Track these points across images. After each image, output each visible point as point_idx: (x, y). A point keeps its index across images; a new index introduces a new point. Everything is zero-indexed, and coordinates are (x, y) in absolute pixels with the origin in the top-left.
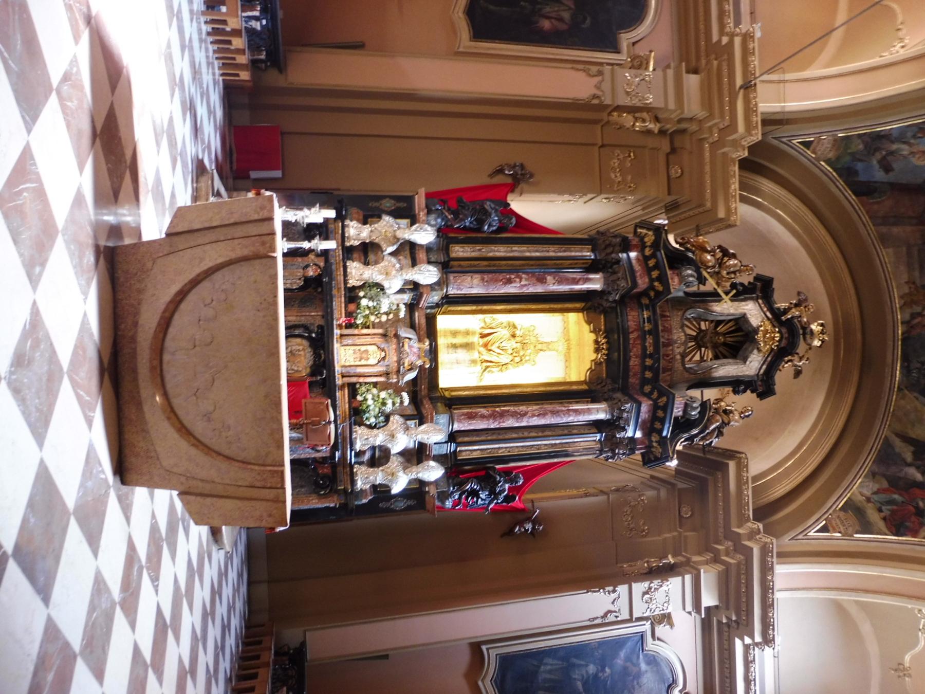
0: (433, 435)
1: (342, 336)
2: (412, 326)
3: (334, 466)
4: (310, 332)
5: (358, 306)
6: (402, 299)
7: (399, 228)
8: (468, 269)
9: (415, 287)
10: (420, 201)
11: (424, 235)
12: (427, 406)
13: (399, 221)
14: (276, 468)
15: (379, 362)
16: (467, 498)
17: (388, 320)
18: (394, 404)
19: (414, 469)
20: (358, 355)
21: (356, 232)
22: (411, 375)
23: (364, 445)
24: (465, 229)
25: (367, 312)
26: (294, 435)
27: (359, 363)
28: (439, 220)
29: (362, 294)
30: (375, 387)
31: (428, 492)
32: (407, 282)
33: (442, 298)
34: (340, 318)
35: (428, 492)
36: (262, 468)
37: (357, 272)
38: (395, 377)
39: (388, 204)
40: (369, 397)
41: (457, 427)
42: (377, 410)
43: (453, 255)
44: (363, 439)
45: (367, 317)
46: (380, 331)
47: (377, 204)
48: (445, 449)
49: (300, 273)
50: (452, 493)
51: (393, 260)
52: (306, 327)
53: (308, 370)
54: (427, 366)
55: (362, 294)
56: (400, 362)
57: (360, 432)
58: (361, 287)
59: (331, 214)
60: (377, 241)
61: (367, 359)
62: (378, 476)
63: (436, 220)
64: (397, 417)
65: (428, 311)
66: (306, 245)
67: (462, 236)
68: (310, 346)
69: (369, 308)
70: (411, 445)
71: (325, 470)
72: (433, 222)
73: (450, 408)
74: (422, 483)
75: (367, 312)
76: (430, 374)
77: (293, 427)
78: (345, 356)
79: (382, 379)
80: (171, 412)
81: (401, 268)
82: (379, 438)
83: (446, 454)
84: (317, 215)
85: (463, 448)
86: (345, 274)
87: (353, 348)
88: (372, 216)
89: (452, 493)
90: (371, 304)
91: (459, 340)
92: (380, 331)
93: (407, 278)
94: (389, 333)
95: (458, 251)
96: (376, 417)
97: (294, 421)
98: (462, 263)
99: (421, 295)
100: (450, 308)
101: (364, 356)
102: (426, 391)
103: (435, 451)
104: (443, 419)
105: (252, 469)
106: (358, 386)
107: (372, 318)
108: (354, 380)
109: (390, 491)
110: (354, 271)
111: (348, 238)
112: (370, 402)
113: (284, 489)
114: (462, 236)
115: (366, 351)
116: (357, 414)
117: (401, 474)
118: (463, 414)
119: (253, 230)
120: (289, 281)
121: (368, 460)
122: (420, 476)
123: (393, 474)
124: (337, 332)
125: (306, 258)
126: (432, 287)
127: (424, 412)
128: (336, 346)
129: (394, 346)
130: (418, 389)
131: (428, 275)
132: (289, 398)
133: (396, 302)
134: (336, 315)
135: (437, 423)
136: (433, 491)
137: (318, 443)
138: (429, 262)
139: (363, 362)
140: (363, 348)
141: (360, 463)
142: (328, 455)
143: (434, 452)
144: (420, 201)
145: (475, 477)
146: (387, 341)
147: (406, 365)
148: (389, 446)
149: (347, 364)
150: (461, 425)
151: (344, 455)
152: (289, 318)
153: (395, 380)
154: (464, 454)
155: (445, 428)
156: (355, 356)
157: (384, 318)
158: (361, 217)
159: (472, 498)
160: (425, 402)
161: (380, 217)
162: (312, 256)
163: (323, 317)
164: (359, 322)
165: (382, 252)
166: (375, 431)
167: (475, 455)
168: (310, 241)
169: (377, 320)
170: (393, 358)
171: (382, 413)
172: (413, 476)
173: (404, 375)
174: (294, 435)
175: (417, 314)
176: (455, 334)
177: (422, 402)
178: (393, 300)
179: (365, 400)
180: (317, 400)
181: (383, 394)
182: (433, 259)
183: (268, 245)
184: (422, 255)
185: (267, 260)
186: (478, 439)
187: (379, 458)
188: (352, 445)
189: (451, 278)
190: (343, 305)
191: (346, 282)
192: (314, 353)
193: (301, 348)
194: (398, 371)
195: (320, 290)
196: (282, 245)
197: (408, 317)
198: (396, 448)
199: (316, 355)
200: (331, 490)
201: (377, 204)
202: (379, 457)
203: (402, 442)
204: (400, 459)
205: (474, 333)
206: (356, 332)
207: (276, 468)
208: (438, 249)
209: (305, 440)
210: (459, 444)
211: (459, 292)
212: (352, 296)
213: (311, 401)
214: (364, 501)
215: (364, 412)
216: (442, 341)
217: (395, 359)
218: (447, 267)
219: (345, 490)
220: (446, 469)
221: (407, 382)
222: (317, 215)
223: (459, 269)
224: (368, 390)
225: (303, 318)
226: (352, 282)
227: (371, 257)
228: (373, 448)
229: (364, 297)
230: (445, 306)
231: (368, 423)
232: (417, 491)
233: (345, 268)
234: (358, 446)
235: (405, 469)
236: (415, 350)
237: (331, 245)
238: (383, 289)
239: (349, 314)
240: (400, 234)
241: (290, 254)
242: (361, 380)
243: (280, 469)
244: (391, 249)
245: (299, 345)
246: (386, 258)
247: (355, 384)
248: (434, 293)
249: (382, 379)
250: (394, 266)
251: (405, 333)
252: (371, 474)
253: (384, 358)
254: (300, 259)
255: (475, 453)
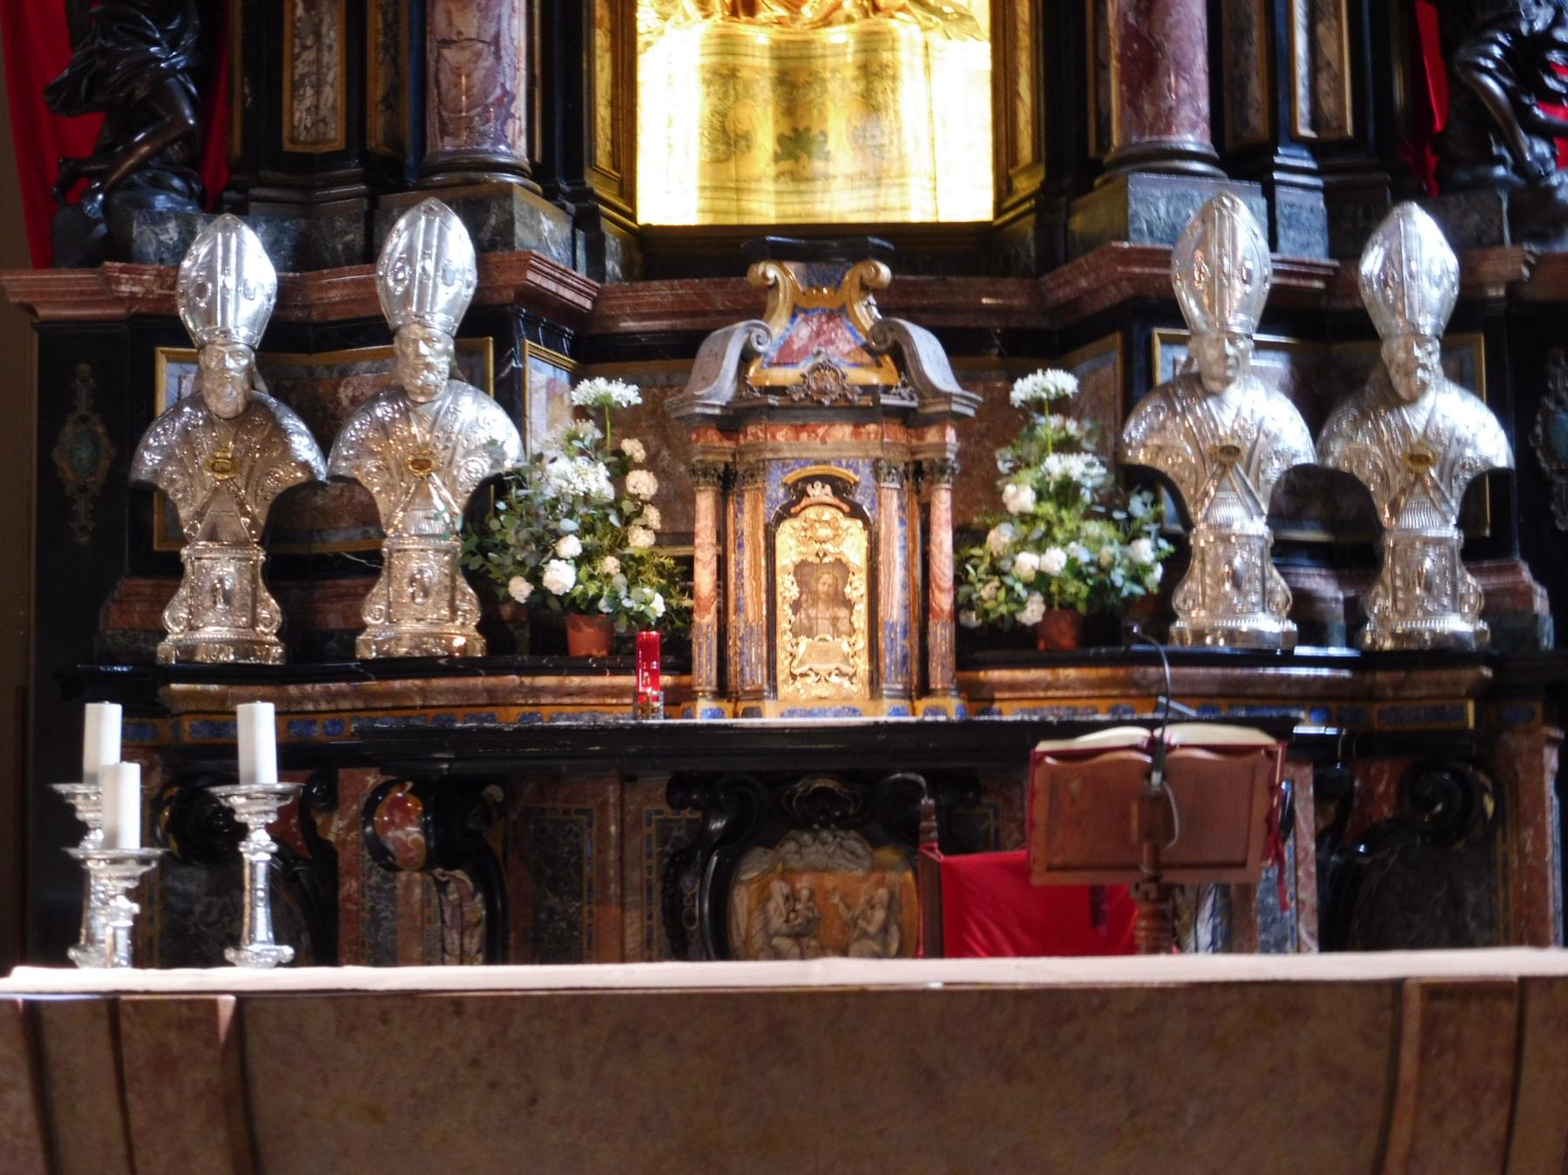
0: (1237, 250)
1: (723, 691)
2: (682, 347)
3: (1362, 744)
4: (703, 841)
5: (578, 607)
6: (552, 393)
7: (197, 401)
8: (408, 68)
9: (493, 335)
10: (63, 294)
11: (240, 276)
12: (1077, 281)
13: (163, 403)
14: (1412, 1027)
15: (855, 512)
16: (1549, 99)
17: (650, 464)
18: (1066, 446)
19: (1393, 351)
20: (822, 613)
21: (216, 608)
22: (929, 352)
23: (1266, 596)
24: (206, 70)
25: (610, 564)
26: (1204, 932)
27: (861, 608)
28: (161, 202)
29: (520, 589)
30: (979, 537)
31: (1513, 286)
32: (467, 368)
33: (550, 195)
34: (630, 698)
35: (1513, 286)
36: (1406, 1099)
37: (417, 607)
38: (932, 436)
39: (80, 455)
40: (1028, 562)
41: (1193, 138)
42: (1093, 528)
43: (335, 134)
44: (1241, 598)
45: (633, 568)
46: (705, 503)
47: (82, 507)
48: (1304, 200)
49: (412, 885)
50: (1520, 166)
51: (356, 429)
52: (679, 861)
53: (887, 855)
54: (885, 272)
55: (520, 589)
56: (861, 410)
57: (1199, 616)
58: (488, 589)
59: (105, 724)
60: (259, 511)
61: (841, 565)
62: (1430, 525)
63: (162, 218)
64: (1135, 430)
65: (612, 266)
66: (258, 849)
67: (242, 90)
68: (771, 843)
69: (586, 558)
70: (1276, 364)
71: (1381, 785)
72: (171, 233)
73: (1096, 168)
74: (1466, 317)
75: (610, 564)
76: (924, 264)
77: (1169, 939)
78: (822, 680)
79: (943, 502)
80: (838, 508)
81: (398, 393)
82: (1239, 519)
83: (1329, 193)
84: (113, 797)
85: (1302, 106)
86: (422, 666)
87: (784, 640)
88: (142, 531)
89: (1520, 166)
90: (571, 546)
91: (762, 123)
92: (705, 503)
93: (443, 364)
94: (715, 458)
95: (315, 107)
96: (1130, 535)
97: (1141, 927)
98: (377, 90)
99: (538, 300)
100: (603, 159)
101: (824, 583)
102: (1010, 284)
103: (1310, 245)
104: (1153, 203)
105: (1411, 1156)
106: (972, 620)
107: (640, 540)
108: (941, 637)
109: (1496, 475)
110: (408, 626)
111: (244, 646)
112: (1055, 559)
113: (1525, 982)
114: (242, 90)
115: (802, 570)
116: (1112, 629)
117: (1416, 419)
118: (1132, 101)
119: (90, 1115)
120: (453, 938)
121: (1342, 583)
122: (1428, 324)
123: (1419, 459)
124: (704, 712)
125: (344, 857)
126: (491, 245)
127: (1112, 296)
128: (771, 716)
129: (782, 435)
130: (997, 326)
131: (434, 263)
132: (1021, 951)
133: (567, 424)
134: (621, 715)
135: (1174, 233)
136: (1512, 261)
137: (1260, 812)
138: (370, 253)
139: (857, 588)
140: (788, 588)
141: (1356, 616)
142: (1307, 772)
143: (1317, 253)
144: (63, 294)
145: (1448, 50)
146: (757, 471)
147: (874, 378)
148: (1274, 471)
149: (862, 665)
150: (1186, 113)
151: (1316, 697)
152: (632, 943)
153: (951, 435)
154: (1328, 105)
155: (1199, 194)
156: (824, 625)
157: (642, 483)
158: (145, 584)
159: (1551, 70)
160: (1064, 293)
161: (148, 494)
162: (336, 828)
163: (628, 779)
164: (658, 606)
165: (312, 484)
166: (1201, 539)
167: (1339, 49)
168: (242, 831)
169: (653, 515)
170: (838, 442)
171: (1109, 505)
172: (1429, 356)
173: (926, 390)
174: (1204, 932)
175: (629, 325)
176: (727, 140)
177: (1071, 305)
178: (547, 436)
179: (1041, 581)
180: (1040, 811)
181: (1019, 496)
182: (355, 236)
183: (172, 1037)
184: (334, 290)
185: (253, 1044)
186: (1256, 34)
187: (1330, 522)
188: (1261, 653)
189: (448, 145)
190: (576, 681)
191: (460, 665)
192: (805, 824)
193: (779, 888)
194: (908, 418)
195: (495, 792)
196: (260, 966)
197: (637, 366)
198: (1289, 436)
199: (817, 814)
200: (1479, 763)
201: (82, 507)
202: (1327, 524)
203: (1260, 409)
204: (1343, 421)
205: (727, 45)
206: (706, 620)
207: (1412, 1027)
208: (307, 208)
209: (1233, 878)
210: (1280, 130)
211: (519, 107)
212: (531, 635)
213: (1046, 848)
214: (1541, 603)
215: (1103, 589)
216: (765, 207)
217: (843, 432)
218: (401, 163)
219: (1486, 695)
220: (1403, 195)
221: (963, 378)
222: (113, 797)
223: (408, 102)
224: (995, 571)
225: (635, 876)
226: (462, 636)
227: (341, 539)
228: (1283, 552)
229: (535, 577)
230: (592, 181)
231: (1159, 571)
232: (1499, 340)
233: (390, 667)
234: (1270, 625)
235: (1395, 400)
236: (804, 332)
237: (259, 728)
238: (495, 488)
239: (622, 652)
240: (228, 399)
241: (315, 931)
242: (943, 601)
243: (1414, 1004)
244: (303, 446)
245: (764, 897)
246: (343, 468)
247: (963, 636)
248: (521, 233)
249: (943, 502)
250: (384, 428)
251: (718, 388)
252: (1413, 566)
253: (841, 488)
254: (350, 886)
255: (1329, 51)
